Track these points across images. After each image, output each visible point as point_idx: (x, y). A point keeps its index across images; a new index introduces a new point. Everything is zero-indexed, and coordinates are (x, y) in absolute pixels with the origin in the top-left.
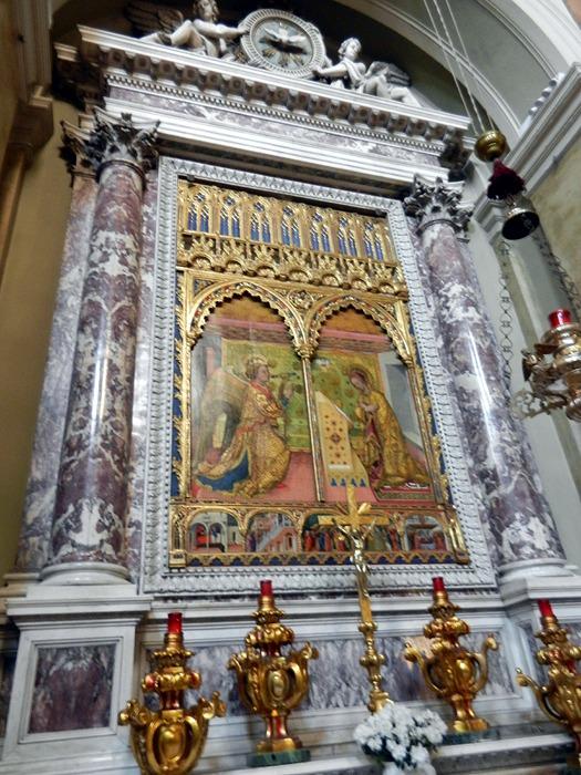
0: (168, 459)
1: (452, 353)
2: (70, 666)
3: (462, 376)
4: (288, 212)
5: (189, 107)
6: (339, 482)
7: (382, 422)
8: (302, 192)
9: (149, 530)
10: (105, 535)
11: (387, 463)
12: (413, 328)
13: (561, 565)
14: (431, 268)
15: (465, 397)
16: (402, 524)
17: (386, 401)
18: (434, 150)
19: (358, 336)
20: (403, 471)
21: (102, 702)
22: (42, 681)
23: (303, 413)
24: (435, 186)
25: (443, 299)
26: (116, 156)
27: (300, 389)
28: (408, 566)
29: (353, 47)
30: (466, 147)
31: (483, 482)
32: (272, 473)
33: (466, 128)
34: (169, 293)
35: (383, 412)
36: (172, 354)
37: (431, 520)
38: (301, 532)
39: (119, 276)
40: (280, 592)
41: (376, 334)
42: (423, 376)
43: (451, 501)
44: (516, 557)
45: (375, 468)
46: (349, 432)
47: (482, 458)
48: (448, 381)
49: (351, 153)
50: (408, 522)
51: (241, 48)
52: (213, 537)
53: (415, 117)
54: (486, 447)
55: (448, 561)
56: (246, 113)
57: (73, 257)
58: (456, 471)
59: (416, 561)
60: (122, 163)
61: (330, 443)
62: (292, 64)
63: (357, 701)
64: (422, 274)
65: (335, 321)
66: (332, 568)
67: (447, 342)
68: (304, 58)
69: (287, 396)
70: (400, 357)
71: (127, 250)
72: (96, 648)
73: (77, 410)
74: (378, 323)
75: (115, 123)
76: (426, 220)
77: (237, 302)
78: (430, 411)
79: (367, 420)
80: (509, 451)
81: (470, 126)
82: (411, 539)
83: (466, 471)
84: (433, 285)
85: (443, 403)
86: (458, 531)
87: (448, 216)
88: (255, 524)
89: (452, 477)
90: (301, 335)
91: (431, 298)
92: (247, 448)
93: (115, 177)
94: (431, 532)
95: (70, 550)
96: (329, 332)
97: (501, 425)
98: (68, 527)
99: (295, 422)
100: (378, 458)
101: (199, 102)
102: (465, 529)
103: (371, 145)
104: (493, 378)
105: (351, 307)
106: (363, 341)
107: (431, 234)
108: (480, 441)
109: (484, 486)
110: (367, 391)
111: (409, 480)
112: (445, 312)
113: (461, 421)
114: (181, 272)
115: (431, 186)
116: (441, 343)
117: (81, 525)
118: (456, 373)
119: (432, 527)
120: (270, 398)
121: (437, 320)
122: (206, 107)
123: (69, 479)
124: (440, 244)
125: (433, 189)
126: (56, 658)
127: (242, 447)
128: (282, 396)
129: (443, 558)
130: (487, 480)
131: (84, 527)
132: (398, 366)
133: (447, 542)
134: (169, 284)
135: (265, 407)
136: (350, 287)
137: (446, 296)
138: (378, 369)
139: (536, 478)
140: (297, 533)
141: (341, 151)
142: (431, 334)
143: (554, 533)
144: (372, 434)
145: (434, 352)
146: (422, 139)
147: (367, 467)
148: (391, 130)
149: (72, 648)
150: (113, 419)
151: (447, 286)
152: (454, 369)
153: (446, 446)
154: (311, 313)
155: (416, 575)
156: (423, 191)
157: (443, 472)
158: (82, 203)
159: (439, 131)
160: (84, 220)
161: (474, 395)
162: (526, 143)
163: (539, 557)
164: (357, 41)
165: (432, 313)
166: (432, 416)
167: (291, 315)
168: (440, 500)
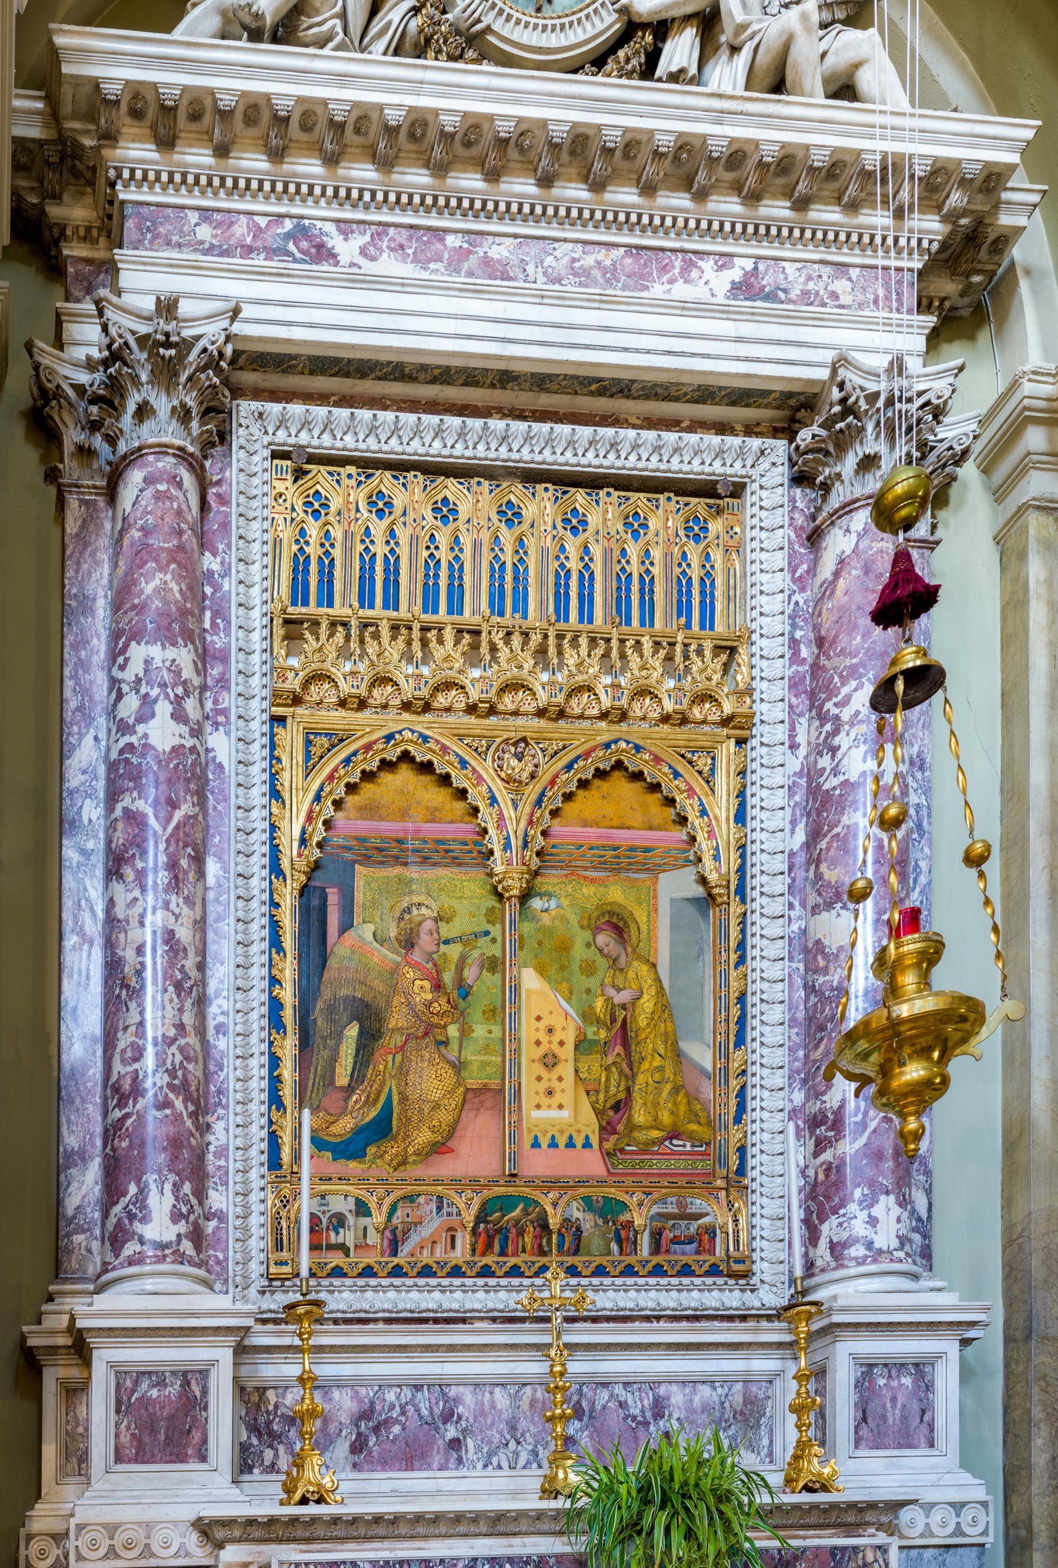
1: (818, 862)
2: (154, 1393)
10: (182, 1227)
14: (820, 642)
17: (658, 980)
21: (197, 1435)
25: (828, 727)
26: (149, 433)
34: (258, 772)
35: (647, 1003)
36: (265, 909)
37: (698, 1204)
45: (614, 1114)
49: (685, 308)
50: (655, 1209)
52: (332, 1234)
55: (714, 1271)
57: (80, 708)
59: (658, 1271)
60: (162, 449)
61: (539, 1069)
64: (796, 658)
70: (703, 880)
72: (185, 1373)
75: (143, 329)
77: (386, 778)
79: (613, 1020)
82: (657, 1236)
86: (742, 1223)
88: (399, 1213)
90: (507, 846)
92: (392, 1084)
98: (131, 1217)
99: (480, 1031)
110: (622, 961)
113: (801, 1015)
120: (438, 986)
123: (124, 1144)
126: (136, 1383)
127: (383, 1084)
131: (155, 1215)
132: (695, 901)
134: (258, 751)
144: (619, 1049)
145: (780, 863)
147: (598, 1113)
154: (532, 791)
160: (93, 612)
163: (875, 1261)
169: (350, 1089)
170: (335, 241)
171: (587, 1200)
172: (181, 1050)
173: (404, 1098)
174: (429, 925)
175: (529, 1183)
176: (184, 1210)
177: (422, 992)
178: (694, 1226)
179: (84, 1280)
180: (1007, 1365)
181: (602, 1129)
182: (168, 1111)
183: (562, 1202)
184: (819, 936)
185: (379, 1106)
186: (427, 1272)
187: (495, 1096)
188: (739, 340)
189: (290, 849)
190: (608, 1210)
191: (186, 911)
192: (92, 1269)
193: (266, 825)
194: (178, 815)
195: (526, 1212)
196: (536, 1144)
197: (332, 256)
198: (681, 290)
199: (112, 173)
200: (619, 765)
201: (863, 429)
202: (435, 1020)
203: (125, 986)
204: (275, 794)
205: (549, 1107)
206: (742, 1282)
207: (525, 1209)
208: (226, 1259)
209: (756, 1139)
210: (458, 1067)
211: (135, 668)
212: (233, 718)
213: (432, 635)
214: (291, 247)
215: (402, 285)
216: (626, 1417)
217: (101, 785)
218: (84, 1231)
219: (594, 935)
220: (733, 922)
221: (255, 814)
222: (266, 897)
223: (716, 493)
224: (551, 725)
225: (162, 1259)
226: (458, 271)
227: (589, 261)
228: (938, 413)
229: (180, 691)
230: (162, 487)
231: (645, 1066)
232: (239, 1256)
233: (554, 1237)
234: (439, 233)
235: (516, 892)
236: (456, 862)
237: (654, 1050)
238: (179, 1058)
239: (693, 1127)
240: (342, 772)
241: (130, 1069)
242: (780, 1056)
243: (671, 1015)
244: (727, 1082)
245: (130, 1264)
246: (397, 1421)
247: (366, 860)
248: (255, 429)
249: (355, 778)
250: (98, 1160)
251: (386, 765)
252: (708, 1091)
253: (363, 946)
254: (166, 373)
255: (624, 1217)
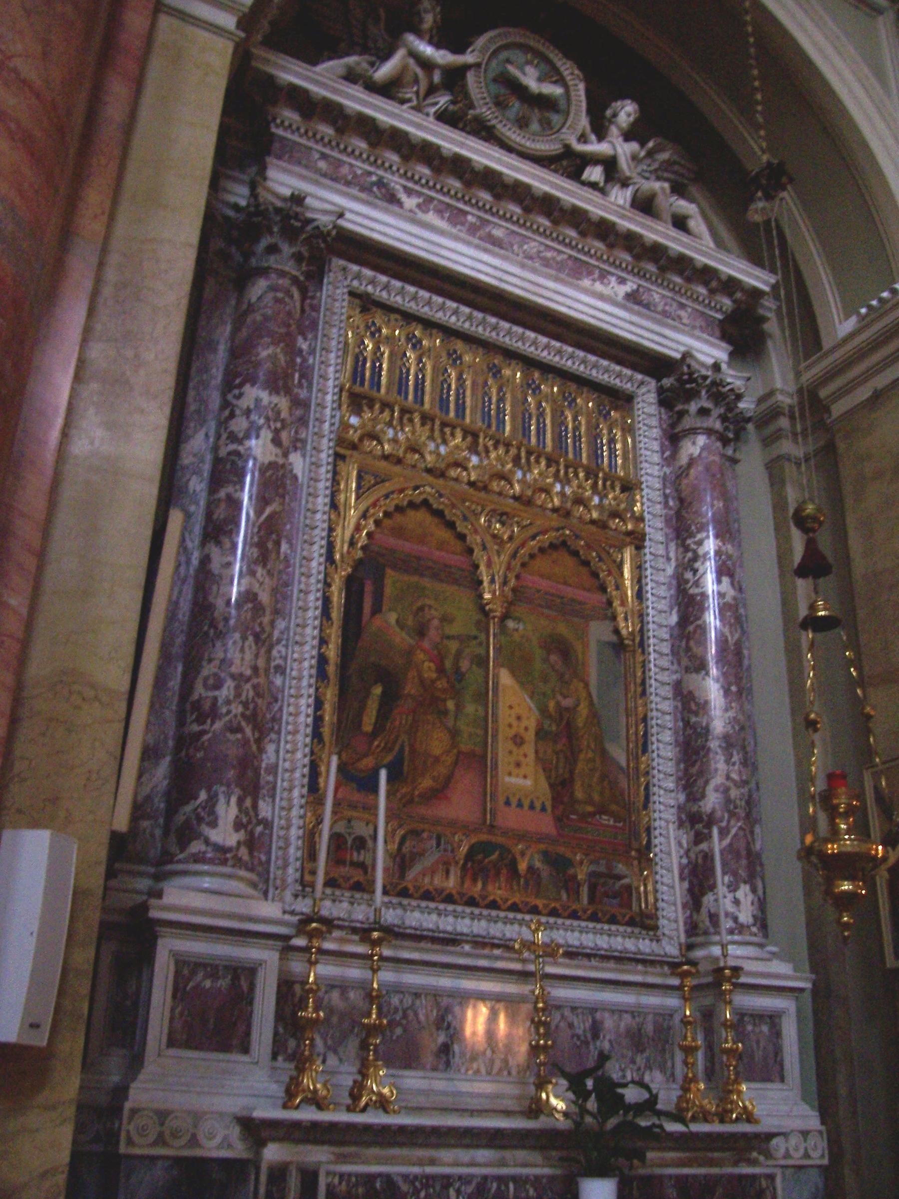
0: (308, 740)
1: (688, 639)
2: (208, 984)
3: (694, 675)
4: (496, 372)
5: (380, 183)
6: (526, 804)
7: (581, 725)
8: (520, 344)
9: (282, 833)
10: (241, 835)
11: (578, 785)
12: (645, 582)
13: (761, 946)
14: (681, 500)
15: (693, 707)
16: (585, 868)
17: (589, 695)
18: (717, 311)
19: (570, 592)
20: (596, 797)
21: (242, 1028)
22: (179, 995)
23: (481, 697)
24: (709, 373)
25: (690, 555)
26: (272, 261)
27: (483, 662)
28: (583, 924)
29: (629, 115)
30: (761, 311)
31: (692, 827)
32: (434, 779)
33: (766, 289)
34: (323, 486)
35: (583, 710)
36: (320, 586)
37: (621, 868)
38: (462, 862)
39: (270, 463)
40: (430, 934)
41: (589, 590)
42: (644, 666)
43: (649, 846)
44: (712, 930)
45: (561, 788)
46: (537, 734)
47: (699, 796)
48: (675, 677)
49: (601, 297)
50: (593, 868)
51: (464, 86)
52: (355, 854)
53: (701, 260)
54: (707, 782)
55: (631, 923)
56: (461, 205)
57: (198, 412)
58: (662, 808)
59: (594, 918)
60: (282, 274)
61: (510, 745)
62: (535, 126)
63: (500, 1070)
64: (666, 505)
65: (541, 564)
66: (494, 913)
67: (684, 621)
68: (556, 119)
69: (463, 670)
70: (617, 631)
71: (283, 421)
72: (235, 969)
73: (210, 661)
74: (595, 575)
75: (279, 204)
76: (687, 423)
77: (411, 513)
78: (645, 719)
79: (561, 718)
80: (734, 793)
81: (775, 287)
82: (593, 889)
83: (674, 811)
84: (682, 529)
85: (661, 705)
86: (650, 887)
87: (718, 425)
88: (407, 844)
89: (656, 815)
90: (492, 581)
91: (672, 546)
92: (404, 737)
93: (271, 295)
94: (618, 885)
95: (203, 848)
96: (532, 580)
97: (731, 756)
98: (200, 819)
99: (470, 709)
100: (567, 776)
101: (396, 178)
102: (659, 886)
103: (629, 287)
104: (734, 688)
105: (564, 544)
106: (573, 600)
107: (694, 446)
108: (701, 773)
109: (692, 833)
110: (567, 677)
111: (602, 810)
112: (689, 575)
113: (681, 739)
114: (343, 458)
115: (704, 372)
116: (674, 619)
117: (216, 819)
118: (687, 670)
119: (619, 877)
120: (441, 670)
121: (674, 582)
122: (405, 187)
123: (200, 755)
124: (700, 468)
125: (705, 378)
126: (193, 973)
127: (397, 737)
128: (457, 670)
129: (627, 918)
130: (699, 826)
131: (221, 822)
132: (610, 644)
133: (634, 899)
134: (324, 472)
135: (433, 682)
136: (568, 514)
137: (695, 552)
138: (586, 646)
139: (757, 829)
140: (457, 863)
141: (586, 291)
142: (663, 605)
143: (762, 904)
144: (564, 740)
145: (664, 634)
146: (702, 290)
147: (551, 786)
148: (662, 270)
149: (211, 965)
150: (255, 681)
151: (699, 536)
152: (685, 662)
153: (653, 681)
154: (510, 547)
155: (591, 936)
156: (692, 380)
157: (646, 806)
158: (214, 321)
159: (730, 285)
160: (215, 350)
161: (704, 706)
162: (849, 347)
163: (740, 933)
164: (636, 107)
165: (670, 570)
166: (646, 726)
167: (484, 548)
168: (635, 845)
169: (374, 734)
170: (403, 197)
171: (545, 854)
172: (255, 687)
173: (413, 750)
174: (436, 622)
175: (504, 833)
176: (245, 820)
177: (429, 670)
178: (618, 885)
179: (141, 861)
180: (815, 1012)
181: (553, 799)
182: (239, 736)
183: (529, 853)
184: (691, 688)
185: (394, 753)
186: (427, 896)
187: (479, 761)
188: (632, 323)
189: (341, 548)
190: (558, 864)
191: (267, 580)
192: (154, 853)
193: (326, 525)
194: (268, 511)
195: (501, 857)
196: (508, 803)
197: (400, 203)
198: (598, 287)
199: (270, 118)
200: (564, 544)
201: (699, 392)
202: (438, 694)
203: (213, 625)
204: (334, 506)
205: (517, 776)
206: (651, 933)
207: (500, 854)
208: (269, 861)
209: (657, 824)
210: (454, 734)
211: (247, 402)
212: (309, 447)
213: (448, 430)
214: (375, 189)
215: (442, 233)
216: (572, 1037)
217: (207, 467)
218: (149, 818)
219: (549, 654)
220: (638, 666)
221: (319, 516)
222: (321, 577)
223: (622, 400)
224: (522, 507)
225: (224, 862)
226: (474, 235)
227: (549, 254)
228: (739, 397)
229: (279, 425)
230: (280, 295)
231: (582, 756)
232: (280, 862)
233: (522, 881)
234: (466, 213)
235: (498, 614)
236: (456, 582)
237: (589, 746)
238: (251, 693)
239: (614, 807)
240: (382, 503)
241: (210, 694)
242: (670, 767)
243: (599, 723)
244: (638, 778)
245: (196, 861)
246: (399, 1024)
247: (394, 567)
248: (340, 276)
249: (391, 509)
250: (168, 759)
251: (412, 505)
252: (623, 783)
253: (389, 624)
254: (291, 234)
255: (571, 871)
